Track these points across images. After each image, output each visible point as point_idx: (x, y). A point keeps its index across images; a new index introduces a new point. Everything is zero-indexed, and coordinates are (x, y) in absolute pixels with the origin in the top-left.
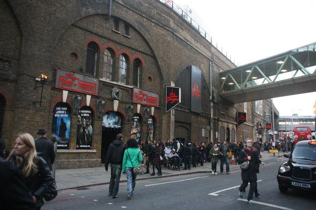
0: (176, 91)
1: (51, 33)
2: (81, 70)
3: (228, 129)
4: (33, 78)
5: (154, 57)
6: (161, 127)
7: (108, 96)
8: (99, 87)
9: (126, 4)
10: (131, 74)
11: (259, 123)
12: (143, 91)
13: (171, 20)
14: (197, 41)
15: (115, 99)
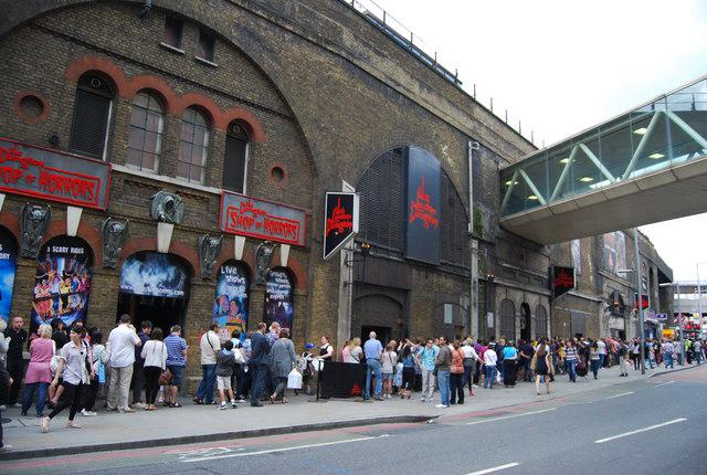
3: (525, 306)
13: (345, 30)
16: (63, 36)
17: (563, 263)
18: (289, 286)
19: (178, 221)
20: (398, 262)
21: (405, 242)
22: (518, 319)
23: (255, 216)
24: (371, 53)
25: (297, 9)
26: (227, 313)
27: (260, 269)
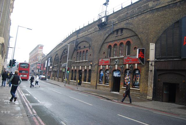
9: (119, 21)
27: (92, 65)
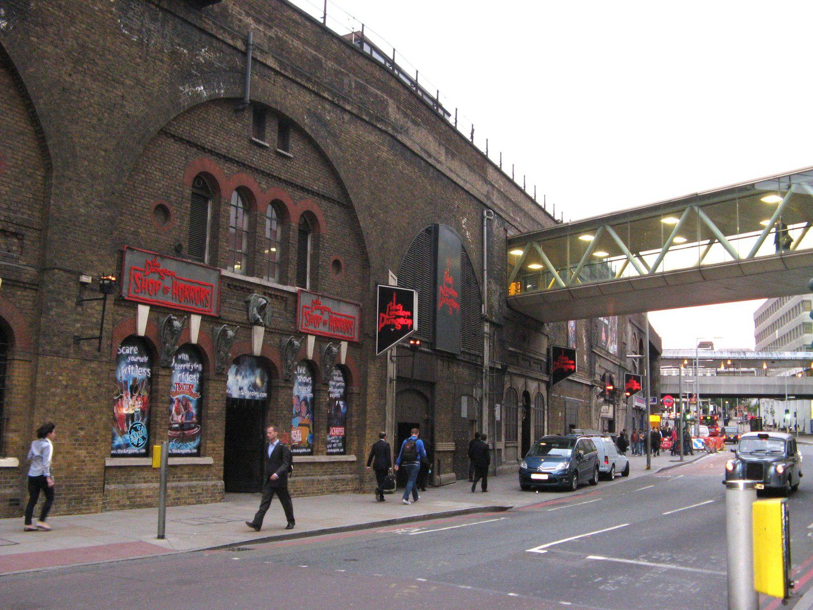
0: (405, 300)
1: (112, 156)
2: (178, 249)
3: (526, 394)
4: (74, 277)
5: (347, 206)
6: (363, 395)
7: (240, 317)
8: (220, 293)
10: (293, 256)
11: (607, 374)
12: (320, 300)
13: (390, 101)
14: (453, 155)
15: (257, 323)
16: (181, 140)
17: (562, 345)
18: (343, 384)
19: (267, 324)
20: (428, 353)
21: (434, 332)
22: (520, 410)
23: (322, 313)
24: (410, 124)
25: (353, 84)
26: (298, 414)
